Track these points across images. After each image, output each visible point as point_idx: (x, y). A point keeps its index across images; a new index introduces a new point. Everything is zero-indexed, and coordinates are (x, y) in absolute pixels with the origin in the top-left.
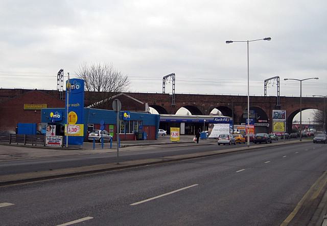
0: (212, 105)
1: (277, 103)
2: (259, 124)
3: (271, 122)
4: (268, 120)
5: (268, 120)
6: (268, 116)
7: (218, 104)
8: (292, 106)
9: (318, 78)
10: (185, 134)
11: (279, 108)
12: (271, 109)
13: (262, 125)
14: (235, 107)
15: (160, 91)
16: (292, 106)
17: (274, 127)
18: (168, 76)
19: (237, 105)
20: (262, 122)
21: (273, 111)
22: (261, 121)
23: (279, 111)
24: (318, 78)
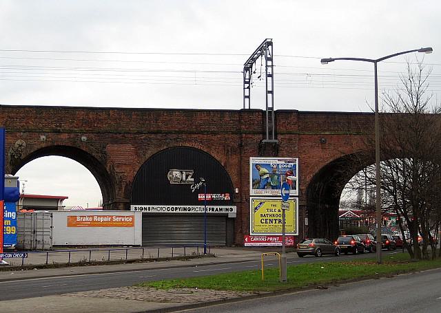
0: (19, 142)
1: (264, 134)
2: (198, 209)
3: (242, 202)
4: (232, 194)
5: (232, 194)
6: (234, 179)
7: (43, 137)
8: (323, 143)
9: (429, 50)
10: (144, 245)
11: (274, 151)
12: (242, 153)
13: (210, 209)
14: (109, 147)
15: (237, 105)
16: (323, 143)
17: (255, 220)
18: (253, 60)
19: (115, 141)
20: (212, 202)
21: (253, 160)
22: (209, 197)
23: (273, 161)
24: (429, 50)
